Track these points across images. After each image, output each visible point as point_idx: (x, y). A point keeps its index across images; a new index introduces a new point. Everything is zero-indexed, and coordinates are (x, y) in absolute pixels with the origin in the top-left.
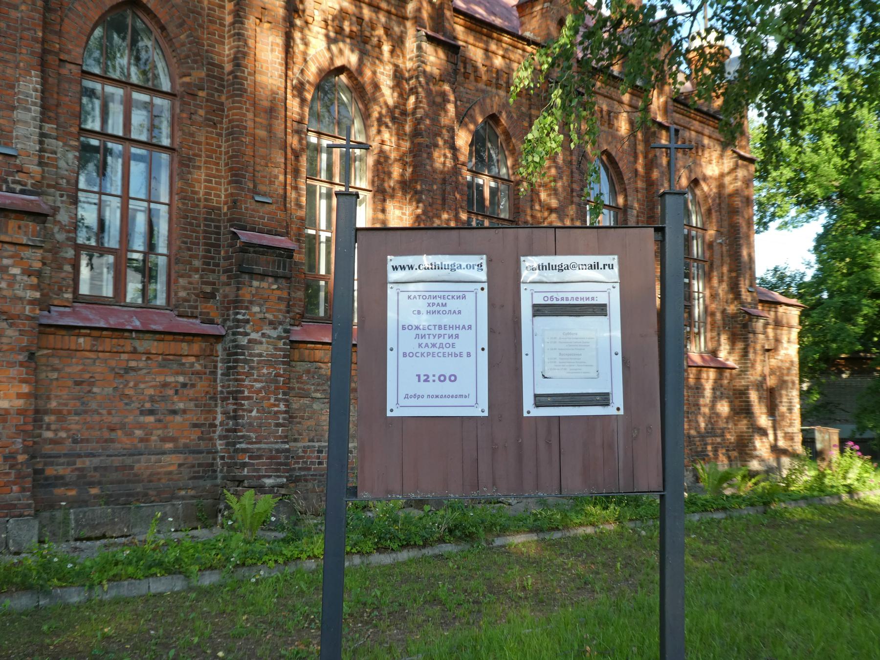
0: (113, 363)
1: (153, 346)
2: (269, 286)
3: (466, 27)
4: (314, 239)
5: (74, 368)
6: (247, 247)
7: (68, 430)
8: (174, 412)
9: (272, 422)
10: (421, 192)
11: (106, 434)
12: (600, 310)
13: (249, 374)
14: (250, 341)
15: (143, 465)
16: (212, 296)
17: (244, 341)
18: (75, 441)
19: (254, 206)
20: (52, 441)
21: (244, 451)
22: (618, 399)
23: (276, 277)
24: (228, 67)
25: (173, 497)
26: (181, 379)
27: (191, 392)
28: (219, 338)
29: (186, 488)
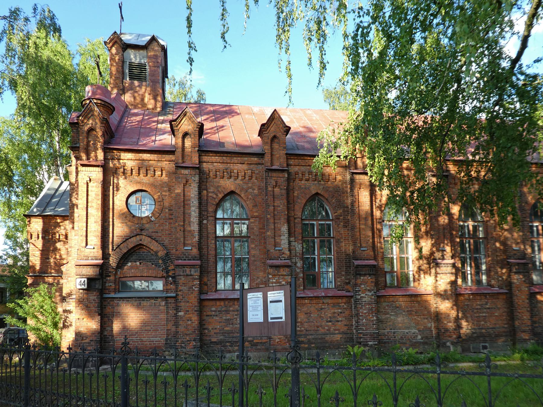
0: (317, 307)
1: (330, 301)
2: (368, 278)
3: (453, 165)
4: (392, 258)
5: (305, 309)
6: (358, 266)
7: (304, 328)
8: (338, 321)
9: (371, 323)
10: (433, 235)
11: (316, 328)
12: (281, 301)
13: (361, 308)
14: (361, 297)
15: (328, 338)
16: (349, 283)
17: (359, 297)
18: (307, 331)
19: (361, 252)
20: (299, 331)
21: (361, 333)
22: (284, 318)
23: (370, 275)
24: (350, 207)
25: (339, 348)
26: (340, 311)
27: (343, 315)
28: (352, 297)
29: (343, 345)
